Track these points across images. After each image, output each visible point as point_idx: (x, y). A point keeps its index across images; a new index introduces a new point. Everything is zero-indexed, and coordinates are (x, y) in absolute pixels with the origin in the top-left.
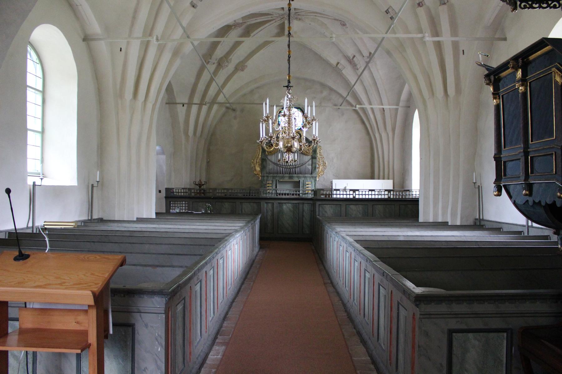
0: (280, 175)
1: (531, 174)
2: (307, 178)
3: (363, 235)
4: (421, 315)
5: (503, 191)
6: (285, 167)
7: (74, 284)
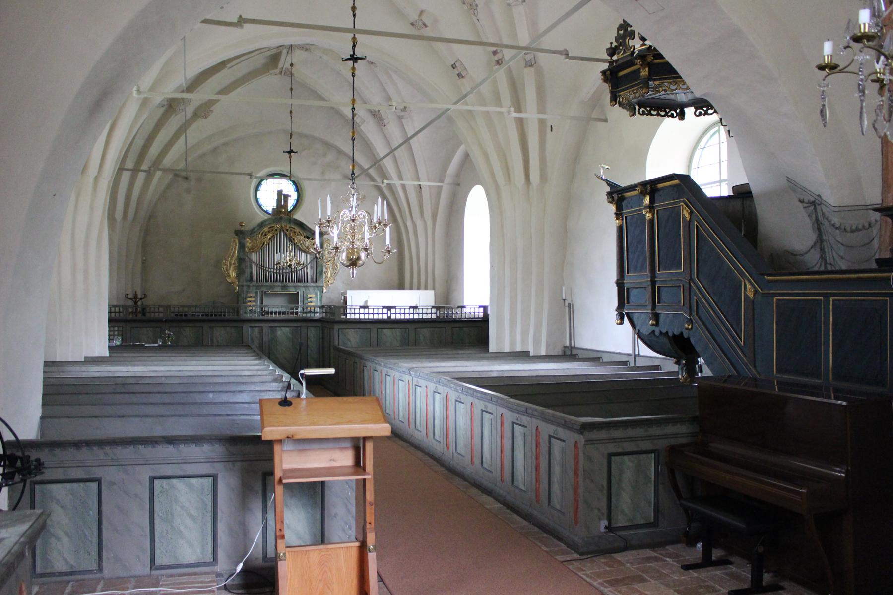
0: (268, 284)
1: (658, 303)
2: (309, 288)
3: (449, 372)
4: (586, 441)
5: (626, 318)
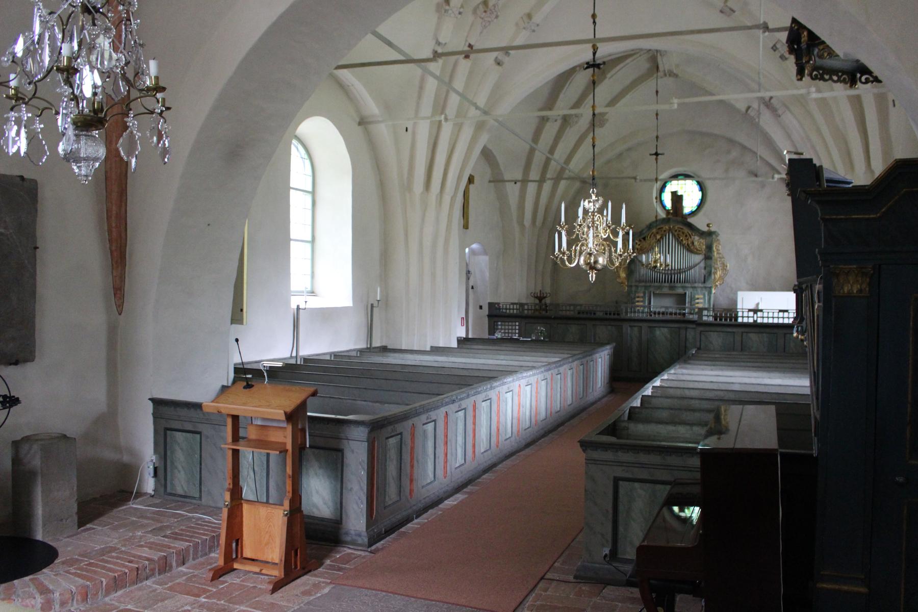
0: (656, 284)
3: (684, 381)
6: (663, 271)
7: (277, 406)
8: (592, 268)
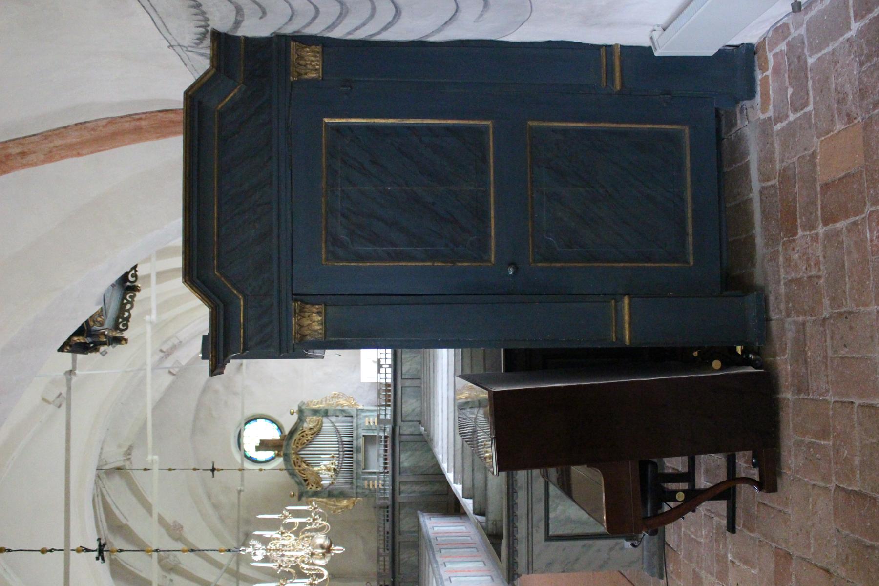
0: (354, 467)
3: (448, 447)
6: (341, 459)
8: (328, 550)
